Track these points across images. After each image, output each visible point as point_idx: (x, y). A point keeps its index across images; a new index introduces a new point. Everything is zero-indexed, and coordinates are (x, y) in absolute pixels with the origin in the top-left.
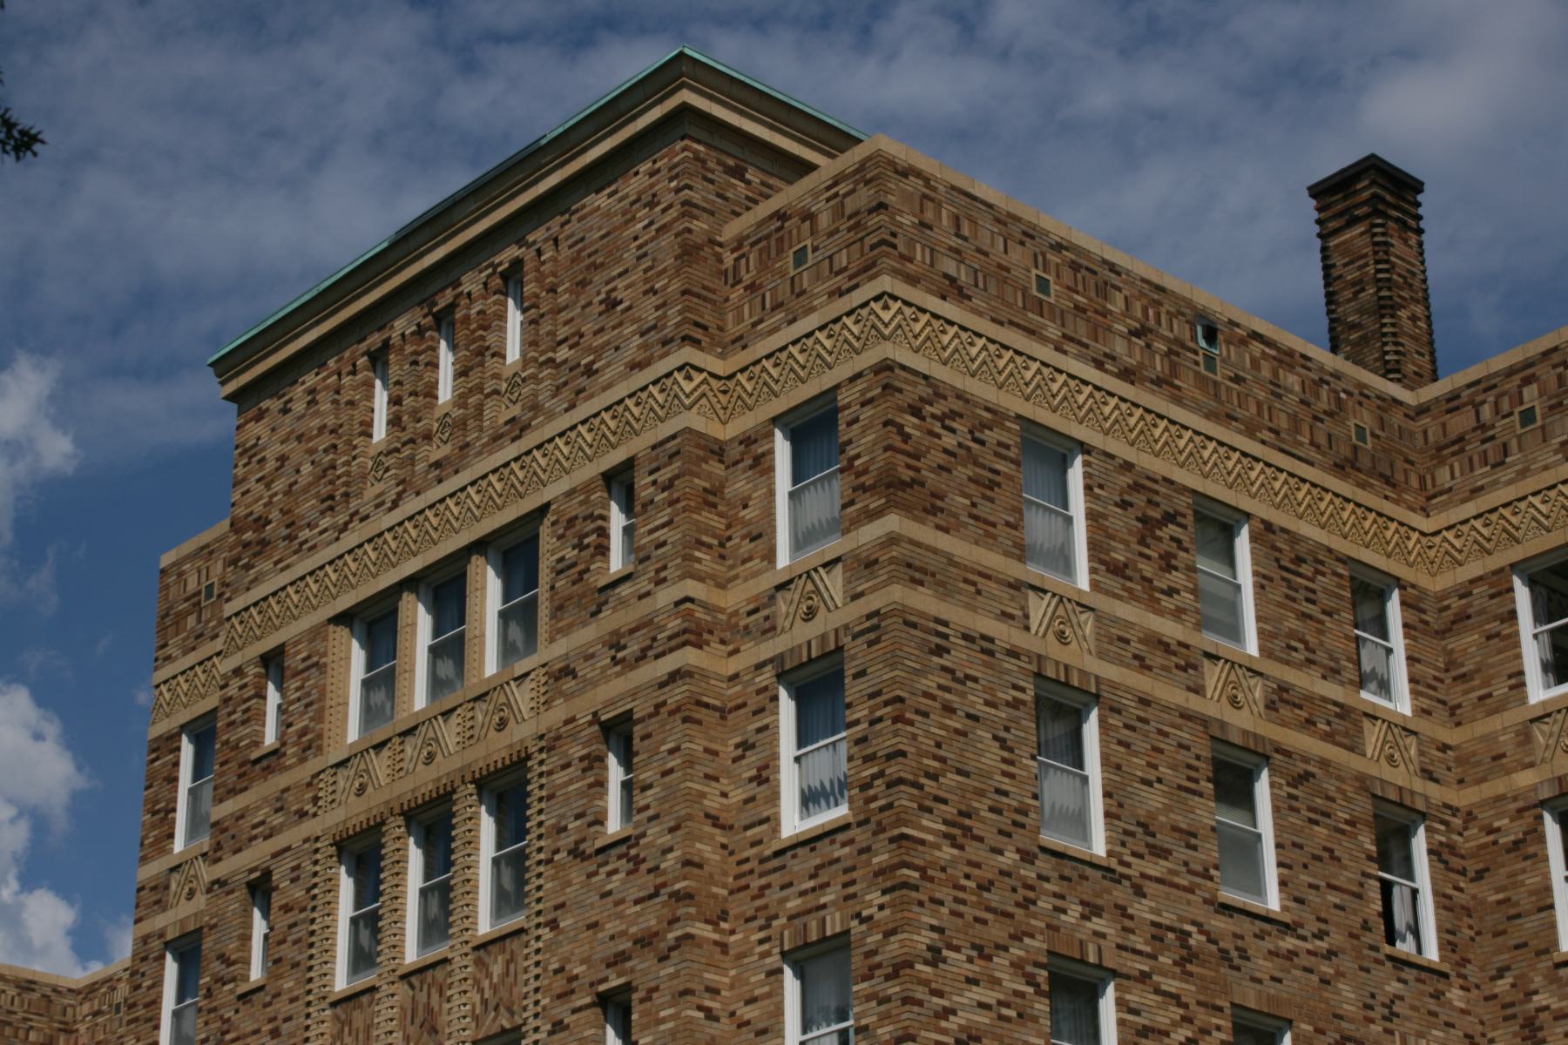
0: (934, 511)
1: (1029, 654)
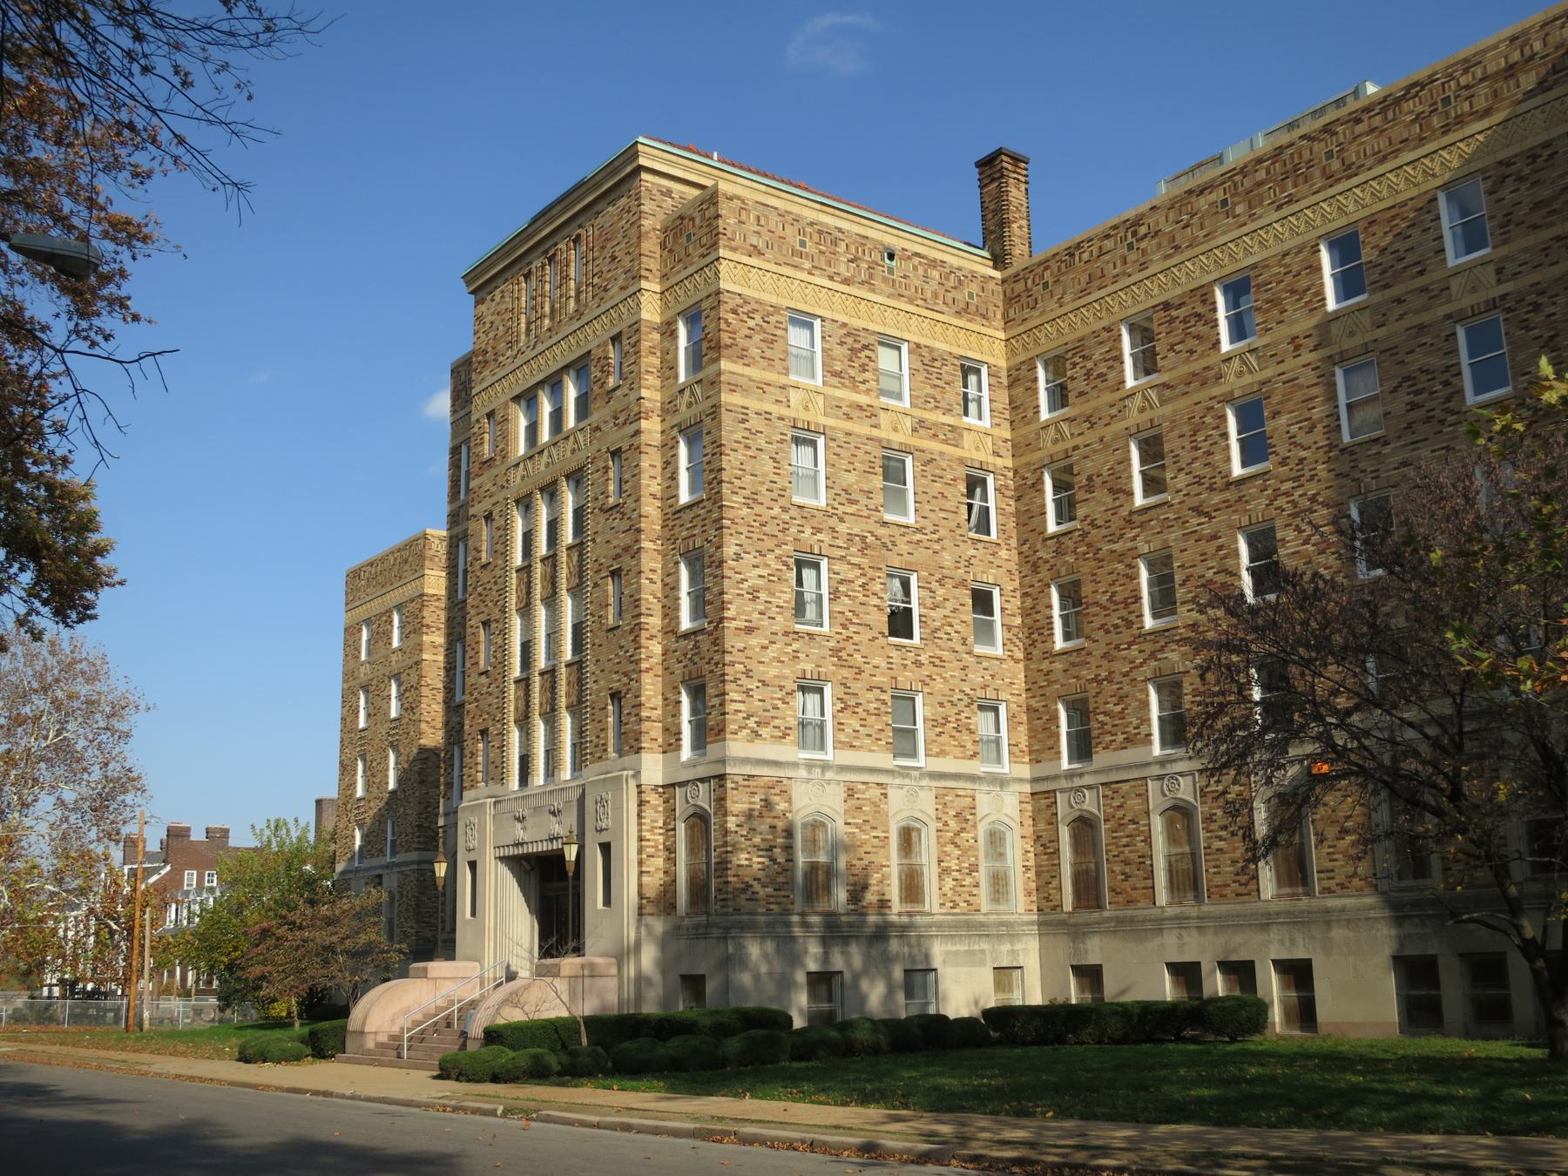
0: (742, 357)
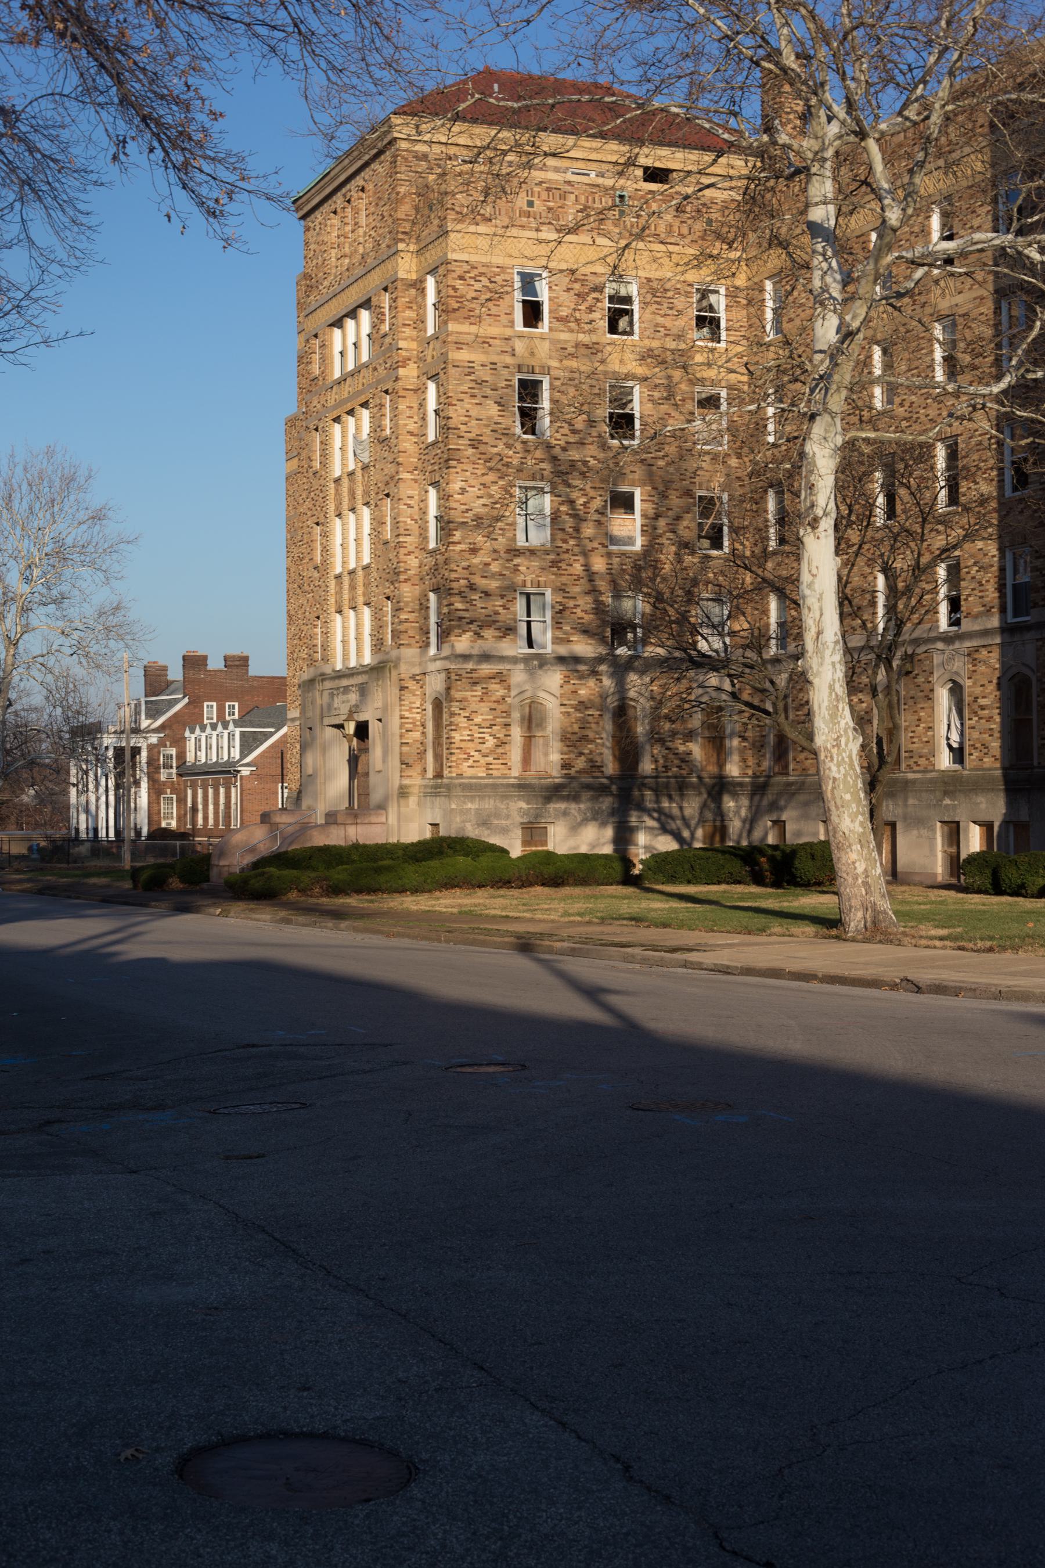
0: (469, 317)
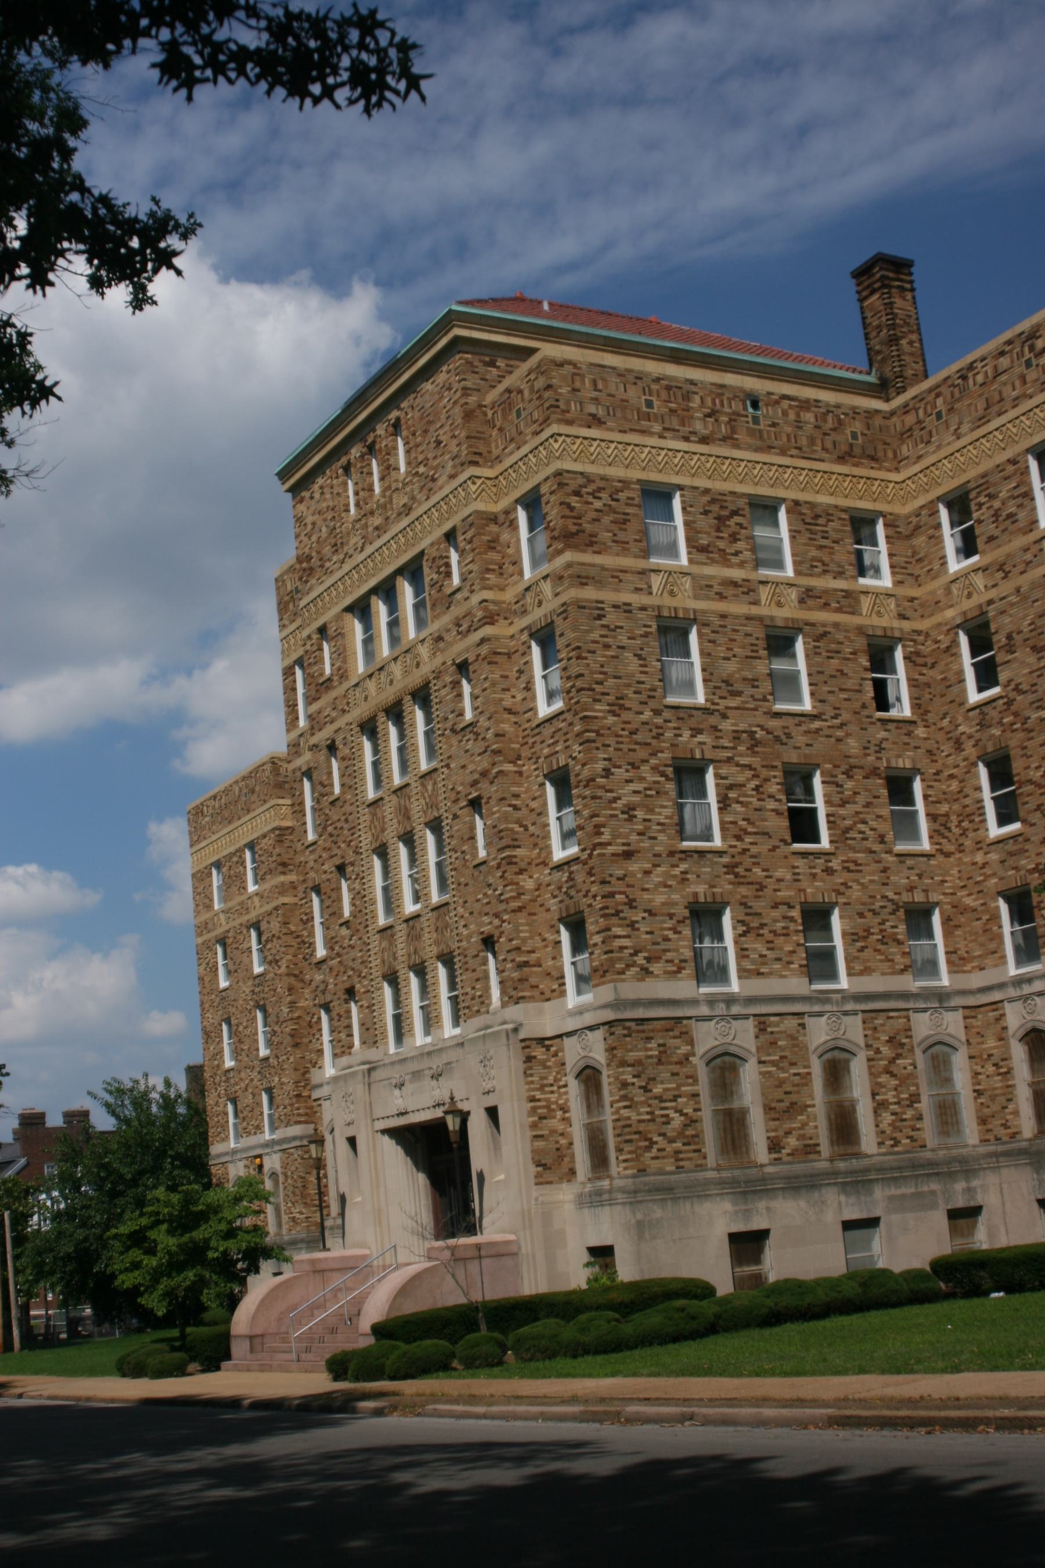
0: (591, 544)
1: (652, 607)
